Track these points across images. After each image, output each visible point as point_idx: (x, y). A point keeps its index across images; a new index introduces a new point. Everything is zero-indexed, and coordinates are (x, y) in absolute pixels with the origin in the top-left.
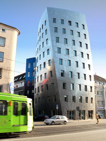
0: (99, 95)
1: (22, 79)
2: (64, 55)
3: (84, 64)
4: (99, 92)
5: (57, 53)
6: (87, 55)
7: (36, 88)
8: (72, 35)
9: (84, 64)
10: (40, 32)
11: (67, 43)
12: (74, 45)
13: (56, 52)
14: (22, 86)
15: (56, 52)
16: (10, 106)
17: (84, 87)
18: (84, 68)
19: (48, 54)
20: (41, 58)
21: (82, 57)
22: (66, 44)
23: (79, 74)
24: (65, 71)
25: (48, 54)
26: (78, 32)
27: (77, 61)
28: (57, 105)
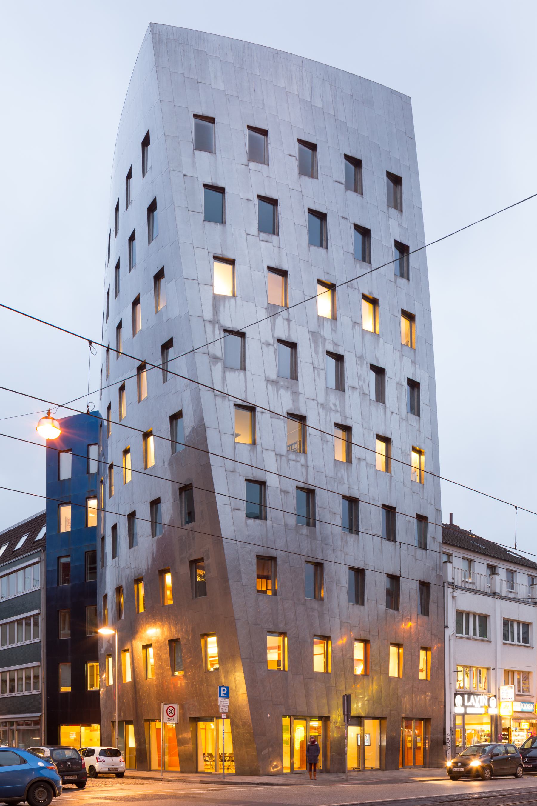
2: (268, 381)
7: (106, 596)
8: (321, 246)
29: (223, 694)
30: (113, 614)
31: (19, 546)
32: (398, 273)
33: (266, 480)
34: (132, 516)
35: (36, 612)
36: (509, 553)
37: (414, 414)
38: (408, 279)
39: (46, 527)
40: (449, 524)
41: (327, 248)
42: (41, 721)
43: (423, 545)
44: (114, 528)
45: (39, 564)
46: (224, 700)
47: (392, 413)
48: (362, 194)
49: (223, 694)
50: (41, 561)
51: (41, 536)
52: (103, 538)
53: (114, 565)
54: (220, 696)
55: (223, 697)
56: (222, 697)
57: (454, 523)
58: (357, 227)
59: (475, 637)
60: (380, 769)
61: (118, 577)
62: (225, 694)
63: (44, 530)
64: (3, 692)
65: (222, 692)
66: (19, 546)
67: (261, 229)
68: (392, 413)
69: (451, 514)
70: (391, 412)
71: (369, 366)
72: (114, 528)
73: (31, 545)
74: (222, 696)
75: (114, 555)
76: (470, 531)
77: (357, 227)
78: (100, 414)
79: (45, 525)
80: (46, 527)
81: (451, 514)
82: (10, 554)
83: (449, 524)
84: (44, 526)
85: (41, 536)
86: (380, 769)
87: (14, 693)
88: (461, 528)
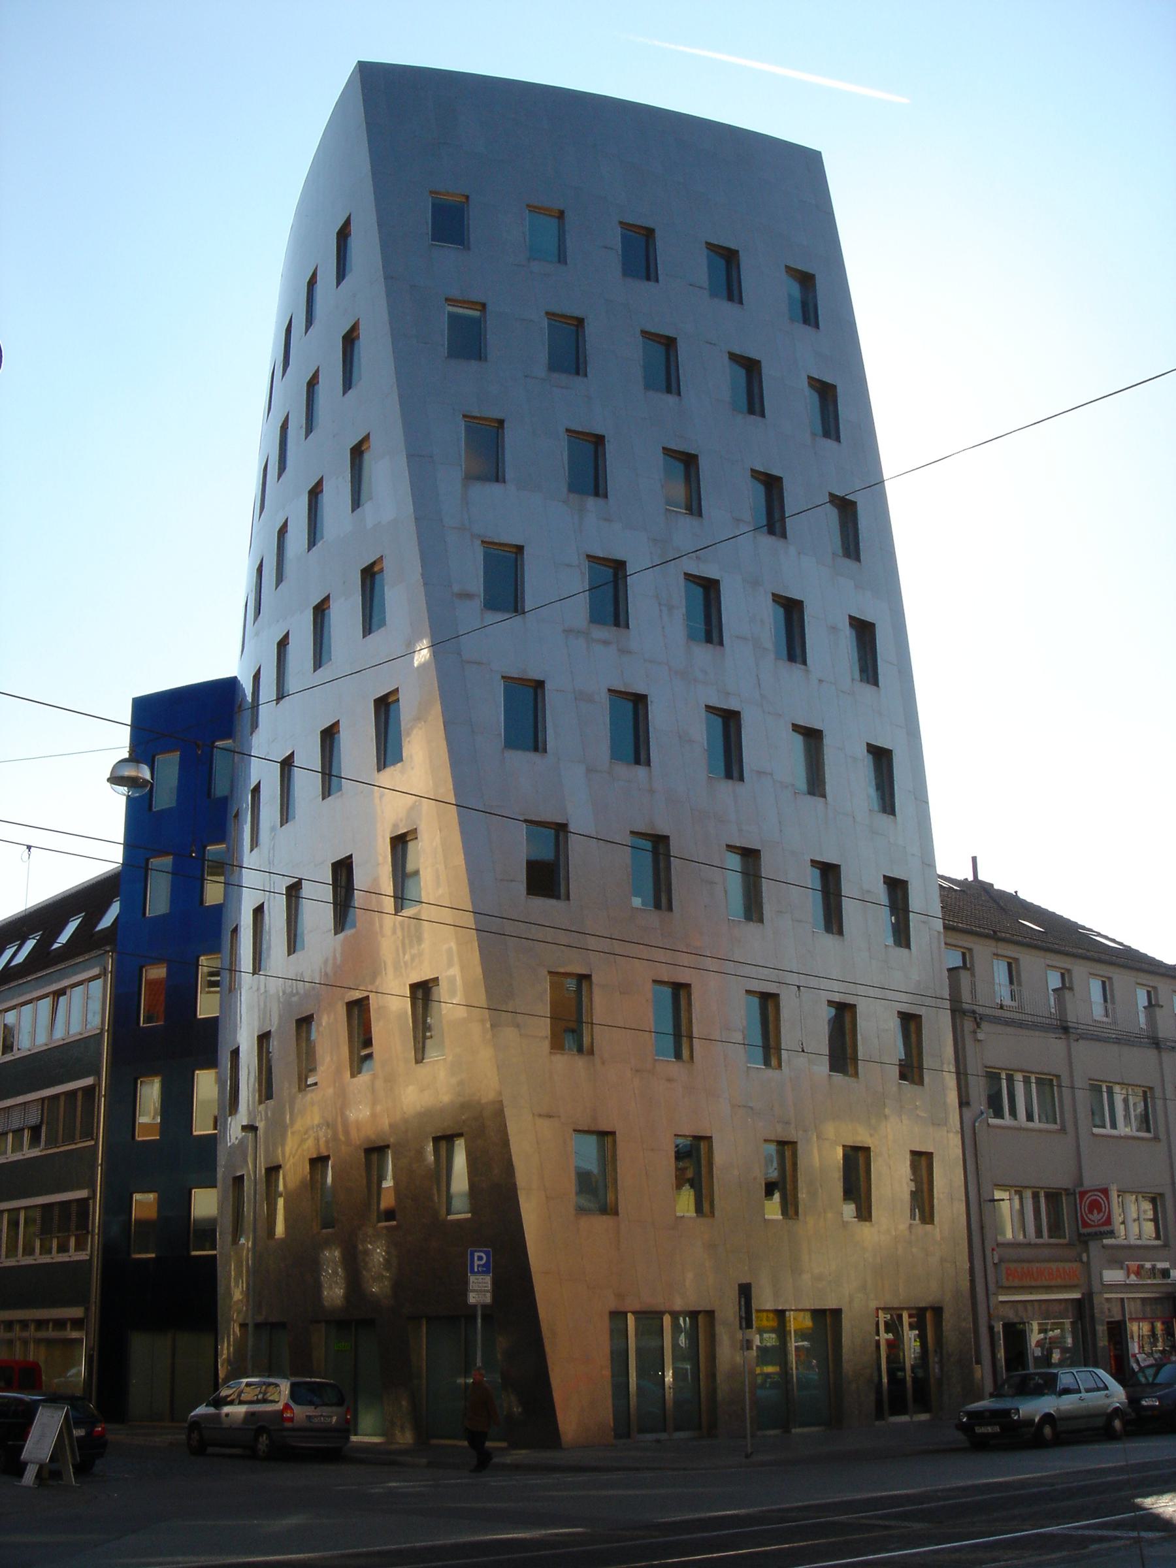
0: (1008, 1120)
1: (85, 942)
2: (568, 632)
3: (812, 737)
4: (1010, 1079)
5: (478, 603)
6: (847, 637)
7: (236, 1053)
8: (669, 390)
9: (812, 737)
10: (309, 321)
11: (598, 489)
12: (694, 507)
13: (468, 596)
14: (59, 1034)
15: (468, 596)
16: (386, 1180)
17: (904, 1169)
18: (816, 784)
19: (371, 619)
20: (293, 683)
21: (833, 920)
22: (591, 502)
23: (750, 855)
24: (580, 820)
25: (371, 619)
26: (797, 728)
27: (733, 705)
28: (480, 1258)
29: (478, 1266)
30: (250, 1089)
31: (64, 938)
32: (819, 429)
33: (567, 820)
34: (294, 891)
35: (89, 1081)
36: (1098, 938)
37: (868, 683)
38: (838, 439)
39: (118, 902)
40: (971, 878)
41: (679, 394)
42: (254, 1102)
43: (902, 935)
44: (259, 911)
45: (99, 982)
46: (480, 1281)
47: (821, 681)
48: (741, 302)
49: (478, 1266)
50: (105, 975)
51: (107, 921)
52: (235, 930)
53: (255, 988)
54: (472, 1272)
55: (478, 1272)
56: (476, 1273)
57: (981, 877)
58: (735, 358)
59: (1030, 1125)
60: (1034, 1356)
61: (264, 1014)
62: (483, 1266)
63: (114, 910)
64: (12, 1250)
65: (477, 1263)
66: (64, 938)
67: (555, 366)
68: (821, 681)
69: (974, 859)
70: (820, 680)
71: (770, 597)
72: (259, 911)
73: (85, 942)
74: (476, 1270)
75: (257, 968)
76: (1016, 892)
77: (735, 358)
78: (239, 681)
79: (119, 898)
80: (118, 902)
81: (974, 859)
82: (41, 960)
83: (971, 878)
84: (115, 900)
85: (107, 921)
86: (1034, 1356)
87: (32, 1257)
88: (996, 887)
